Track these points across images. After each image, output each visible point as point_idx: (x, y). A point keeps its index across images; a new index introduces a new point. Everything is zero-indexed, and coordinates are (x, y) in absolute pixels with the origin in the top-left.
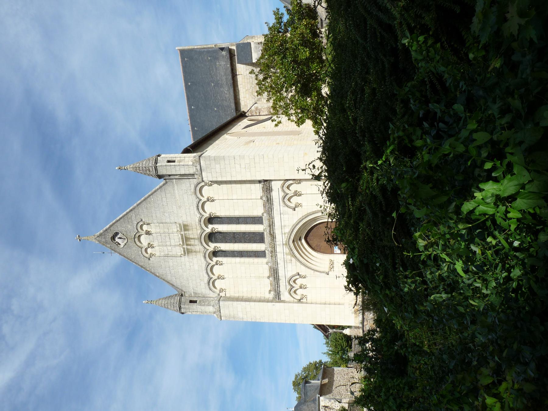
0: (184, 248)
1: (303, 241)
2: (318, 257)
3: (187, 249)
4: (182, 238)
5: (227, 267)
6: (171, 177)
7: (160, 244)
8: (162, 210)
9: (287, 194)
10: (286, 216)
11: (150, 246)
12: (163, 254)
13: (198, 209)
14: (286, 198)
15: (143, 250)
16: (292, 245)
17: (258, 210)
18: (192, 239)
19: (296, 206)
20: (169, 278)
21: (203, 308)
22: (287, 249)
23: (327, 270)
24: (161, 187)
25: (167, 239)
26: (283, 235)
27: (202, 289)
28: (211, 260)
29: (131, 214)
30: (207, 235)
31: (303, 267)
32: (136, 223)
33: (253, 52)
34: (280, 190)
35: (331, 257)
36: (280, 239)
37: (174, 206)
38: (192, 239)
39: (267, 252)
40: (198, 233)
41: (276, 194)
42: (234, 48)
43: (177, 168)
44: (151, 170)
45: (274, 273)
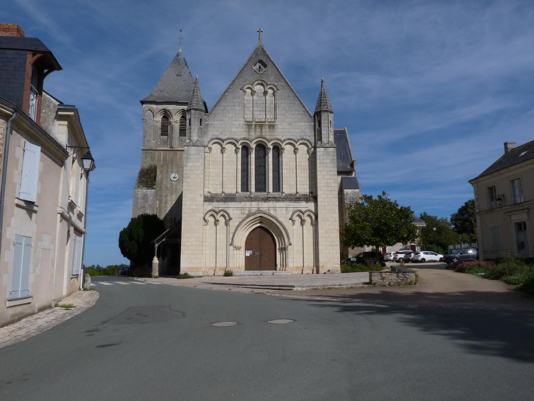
0: (252, 122)
1: (259, 225)
3: (252, 125)
4: (262, 122)
5: (232, 158)
8: (287, 109)
9: (303, 214)
10: (284, 212)
11: (253, 93)
12: (246, 102)
13: (289, 139)
14: (300, 214)
15: (250, 86)
16: (258, 215)
17: (287, 188)
18: (261, 130)
20: (223, 104)
21: (196, 131)
23: (234, 244)
24: (307, 112)
25: (260, 109)
27: (212, 133)
28: (241, 144)
29: (284, 82)
30: (264, 145)
31: (237, 224)
32: (276, 84)
34: (307, 209)
35: (243, 248)
36: (265, 206)
37: (290, 120)
38: (261, 130)
39: (248, 193)
41: (303, 206)
42: (353, 176)
43: (326, 129)
44: (326, 107)
45: (230, 198)
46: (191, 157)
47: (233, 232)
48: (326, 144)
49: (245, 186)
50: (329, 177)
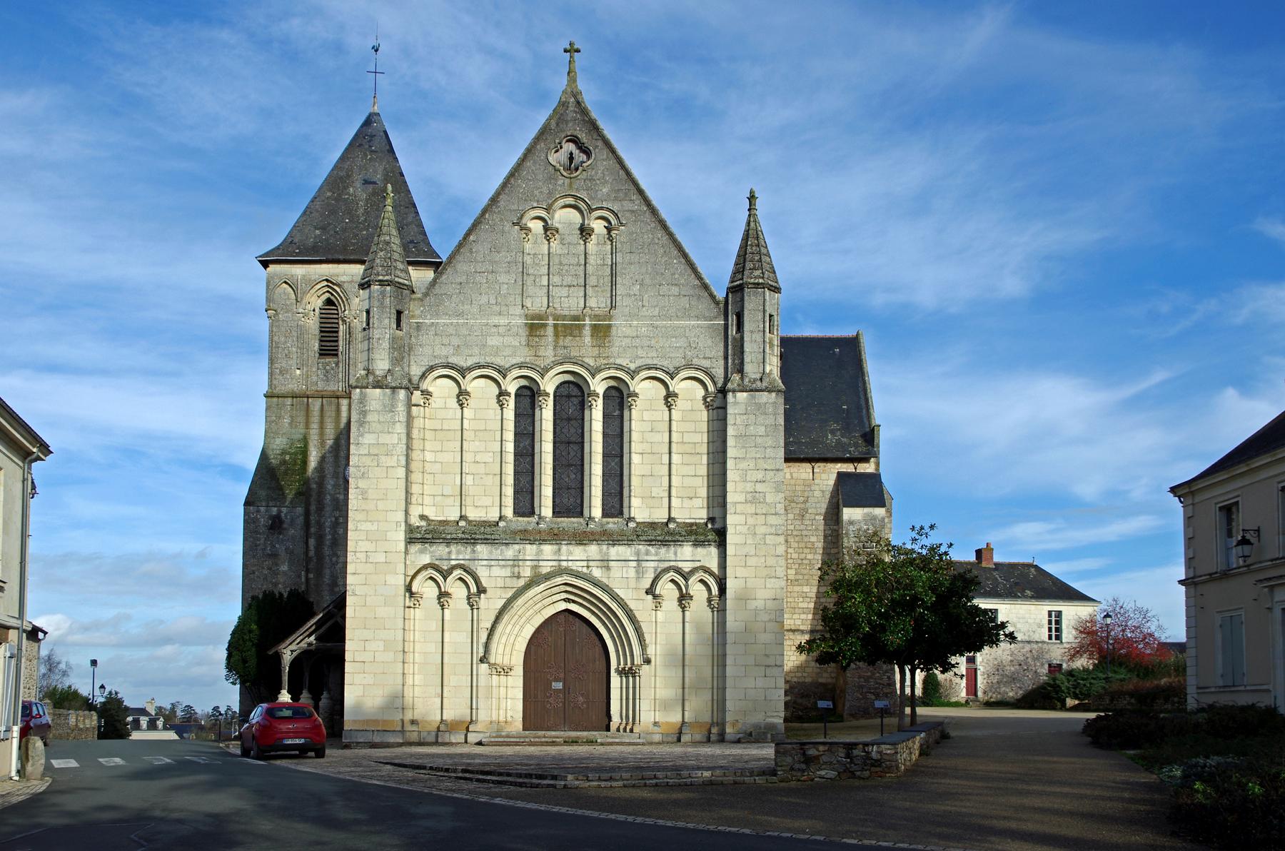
1: (563, 606)
2: (519, 639)
5: (491, 419)
6: (732, 319)
7: (555, 260)
8: (648, 281)
12: (528, 260)
17: (641, 509)
19: (655, 597)
22: (549, 570)
25: (568, 280)
26: (585, 564)
31: (500, 603)
33: (866, 510)
34: (698, 564)
36: (576, 556)
39: (534, 519)
40: (586, 360)
41: (686, 555)
46: (369, 418)
47: (489, 626)
48: (755, 380)
49: (525, 500)
50: (760, 476)
